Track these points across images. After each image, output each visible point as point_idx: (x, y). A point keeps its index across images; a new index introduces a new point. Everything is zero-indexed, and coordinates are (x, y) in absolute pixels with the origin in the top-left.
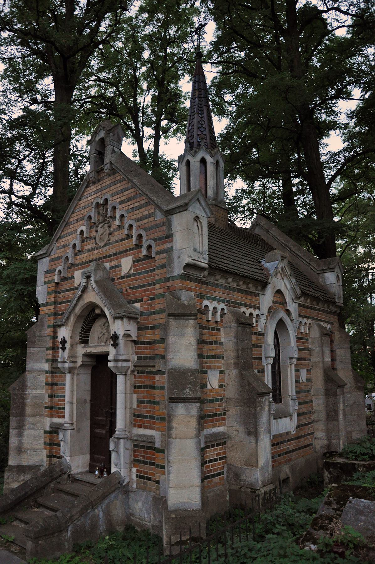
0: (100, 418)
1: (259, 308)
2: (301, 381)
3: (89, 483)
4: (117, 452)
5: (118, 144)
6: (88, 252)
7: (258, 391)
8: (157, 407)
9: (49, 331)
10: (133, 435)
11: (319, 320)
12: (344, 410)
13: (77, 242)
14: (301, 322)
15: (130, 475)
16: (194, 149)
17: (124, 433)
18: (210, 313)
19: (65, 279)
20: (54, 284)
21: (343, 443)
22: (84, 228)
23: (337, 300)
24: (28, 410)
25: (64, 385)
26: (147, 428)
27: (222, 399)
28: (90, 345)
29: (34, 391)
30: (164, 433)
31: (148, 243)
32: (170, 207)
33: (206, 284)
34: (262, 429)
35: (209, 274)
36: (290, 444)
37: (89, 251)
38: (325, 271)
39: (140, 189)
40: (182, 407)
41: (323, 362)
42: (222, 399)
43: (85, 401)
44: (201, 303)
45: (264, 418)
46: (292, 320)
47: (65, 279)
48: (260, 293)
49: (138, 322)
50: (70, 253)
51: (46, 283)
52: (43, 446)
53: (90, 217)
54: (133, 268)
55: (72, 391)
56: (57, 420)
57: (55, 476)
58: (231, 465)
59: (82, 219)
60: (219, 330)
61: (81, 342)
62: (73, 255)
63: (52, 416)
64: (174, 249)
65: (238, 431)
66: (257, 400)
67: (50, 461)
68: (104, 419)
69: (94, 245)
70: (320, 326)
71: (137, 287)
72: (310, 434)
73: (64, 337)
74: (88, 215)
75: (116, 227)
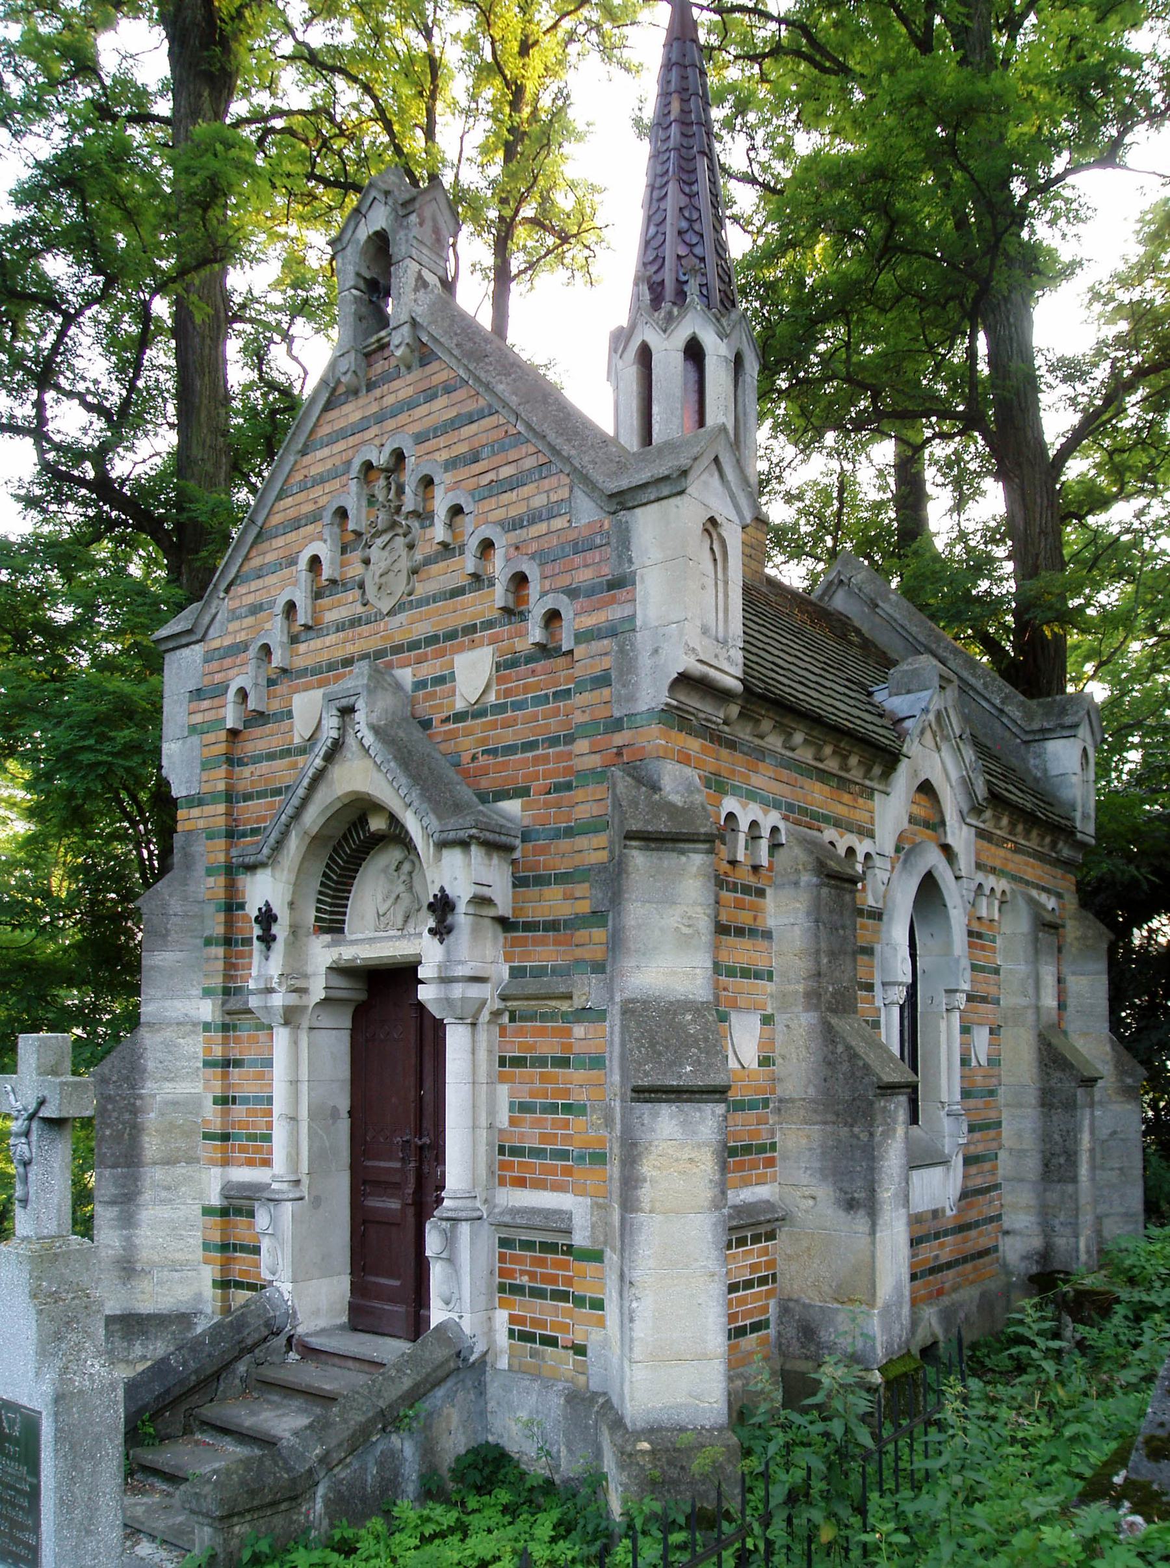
0: (383, 1164)
1: (871, 835)
2: (974, 1063)
3: (355, 1359)
4: (451, 1260)
5: (434, 257)
6: (338, 631)
7: (880, 1079)
8: (577, 1123)
9: (215, 885)
10: (497, 1210)
11: (1027, 883)
12: (1092, 1150)
13: (302, 599)
14: (980, 885)
15: (490, 1331)
16: (666, 306)
17: (468, 1203)
18: (742, 838)
19: (259, 718)
20: (223, 735)
21: (1087, 1247)
22: (323, 549)
23: (1078, 824)
24: (152, 1146)
25: (269, 1063)
26: (545, 1188)
27: (766, 1103)
28: (349, 935)
29: (168, 1086)
30: (601, 1200)
31: (549, 603)
32: (624, 483)
33: (732, 745)
34: (887, 1193)
35: (741, 714)
36: (942, 1245)
37: (340, 627)
38: (1045, 734)
39: (517, 416)
40: (671, 1118)
41: (1037, 1008)
42: (766, 1103)
43: (334, 1113)
44: (718, 805)
45: (893, 1157)
46: (957, 878)
47: (259, 718)
48: (876, 786)
49: (514, 862)
50: (275, 631)
51: (193, 729)
52: (200, 1253)
53: (342, 513)
54: (495, 688)
55: (294, 1083)
56: (243, 1174)
57: (249, 1342)
58: (790, 1300)
59: (315, 517)
60: (761, 893)
61: (320, 928)
62: (285, 639)
63: (225, 1163)
64: (639, 623)
65: (814, 1198)
66: (877, 1105)
67: (225, 1299)
68: (398, 1165)
69: (359, 609)
70: (1033, 903)
71: (510, 750)
72: (991, 1220)
73: (267, 904)
74: (335, 506)
75: (436, 547)
